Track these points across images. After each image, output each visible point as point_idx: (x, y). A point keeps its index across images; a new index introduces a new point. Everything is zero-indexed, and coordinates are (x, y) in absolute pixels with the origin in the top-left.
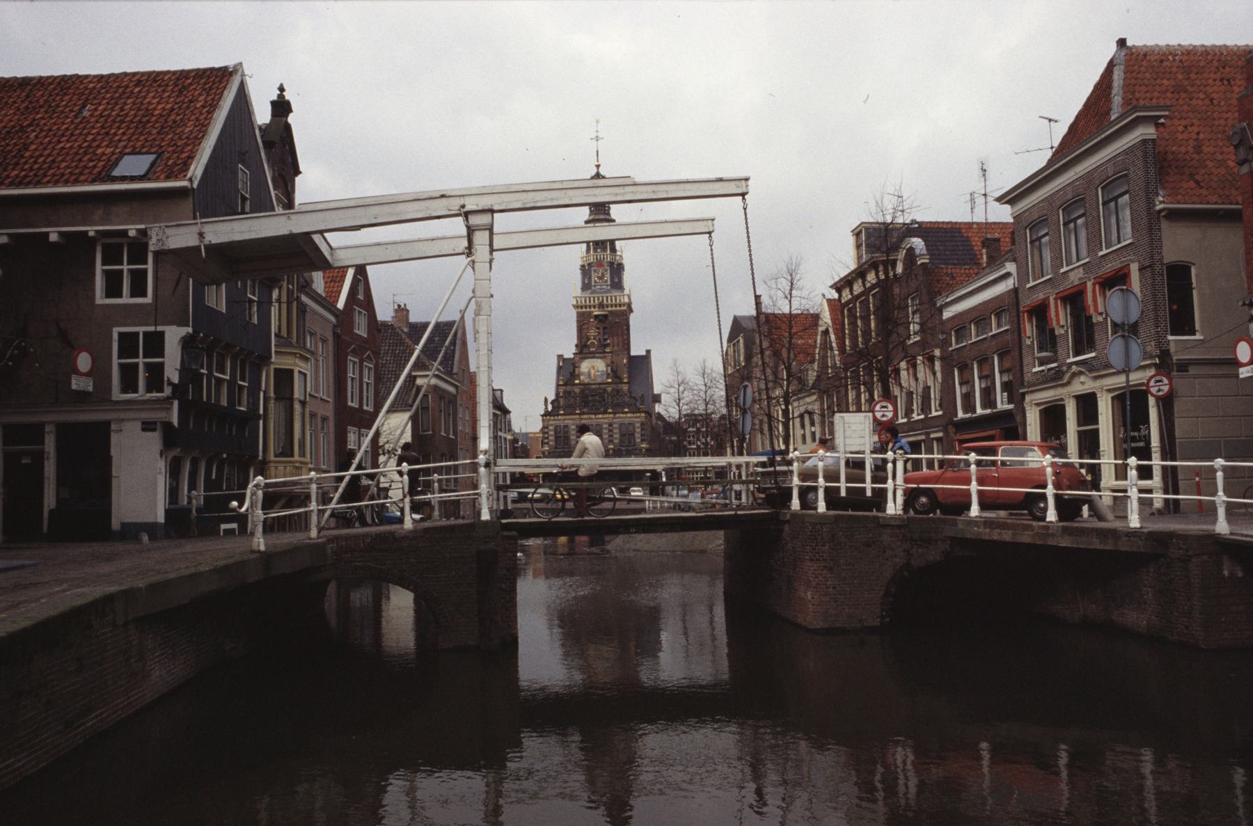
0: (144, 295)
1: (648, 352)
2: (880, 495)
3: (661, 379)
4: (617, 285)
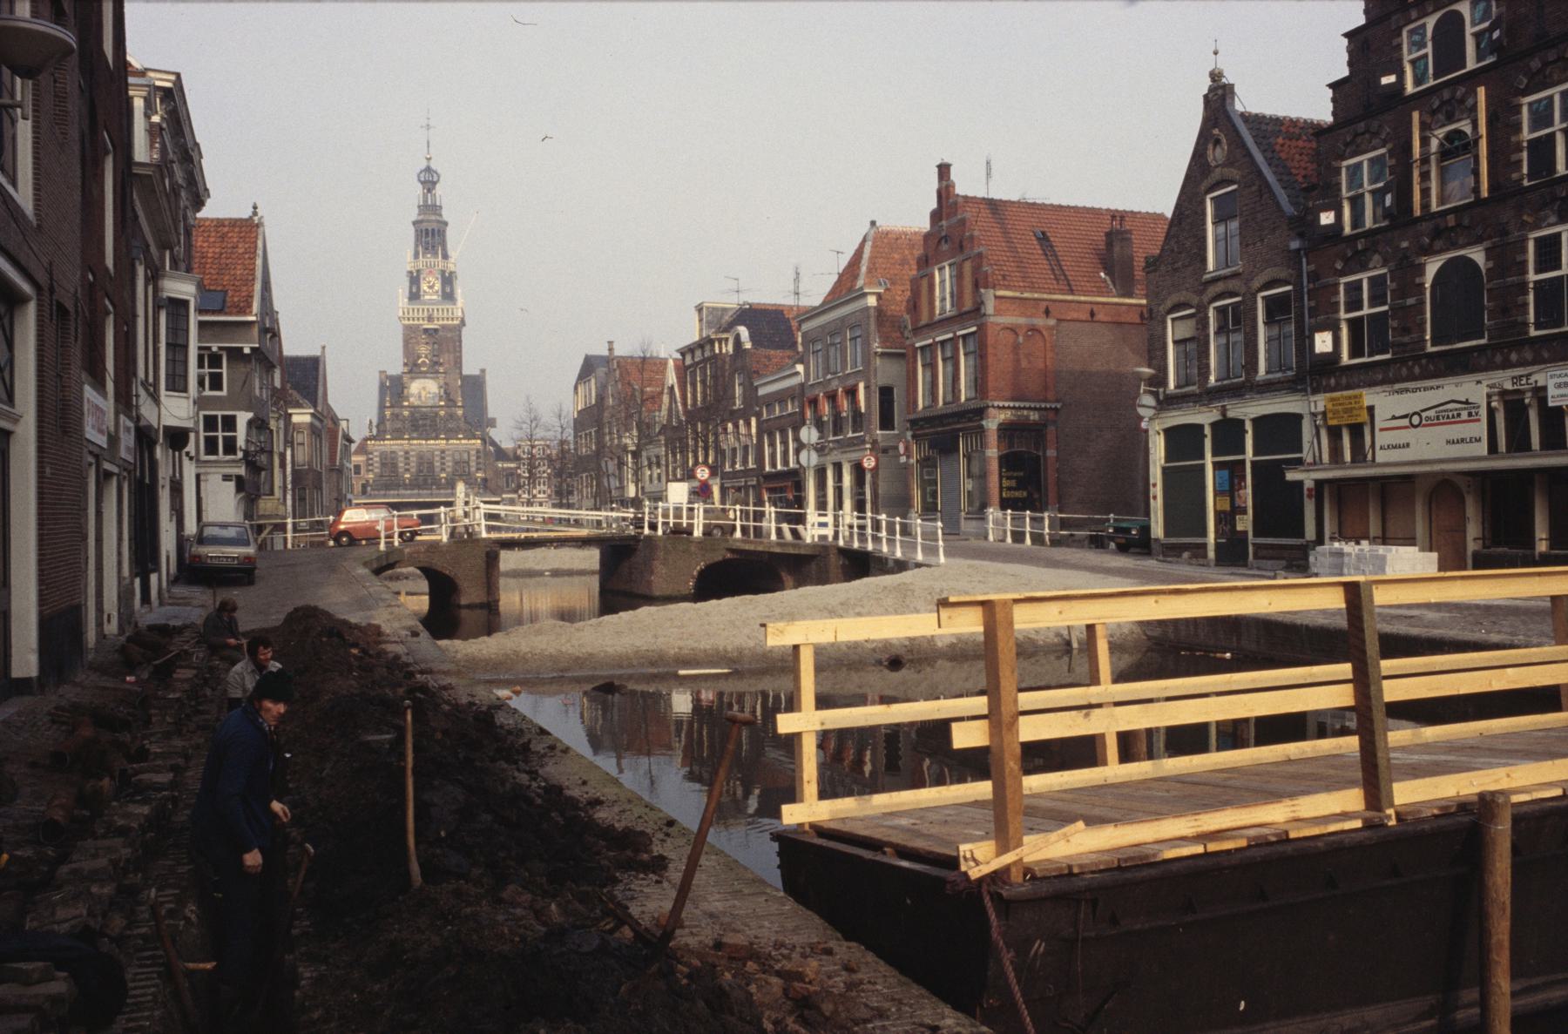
0: (220, 389)
1: (483, 371)
2: (691, 526)
3: (496, 404)
4: (449, 296)
